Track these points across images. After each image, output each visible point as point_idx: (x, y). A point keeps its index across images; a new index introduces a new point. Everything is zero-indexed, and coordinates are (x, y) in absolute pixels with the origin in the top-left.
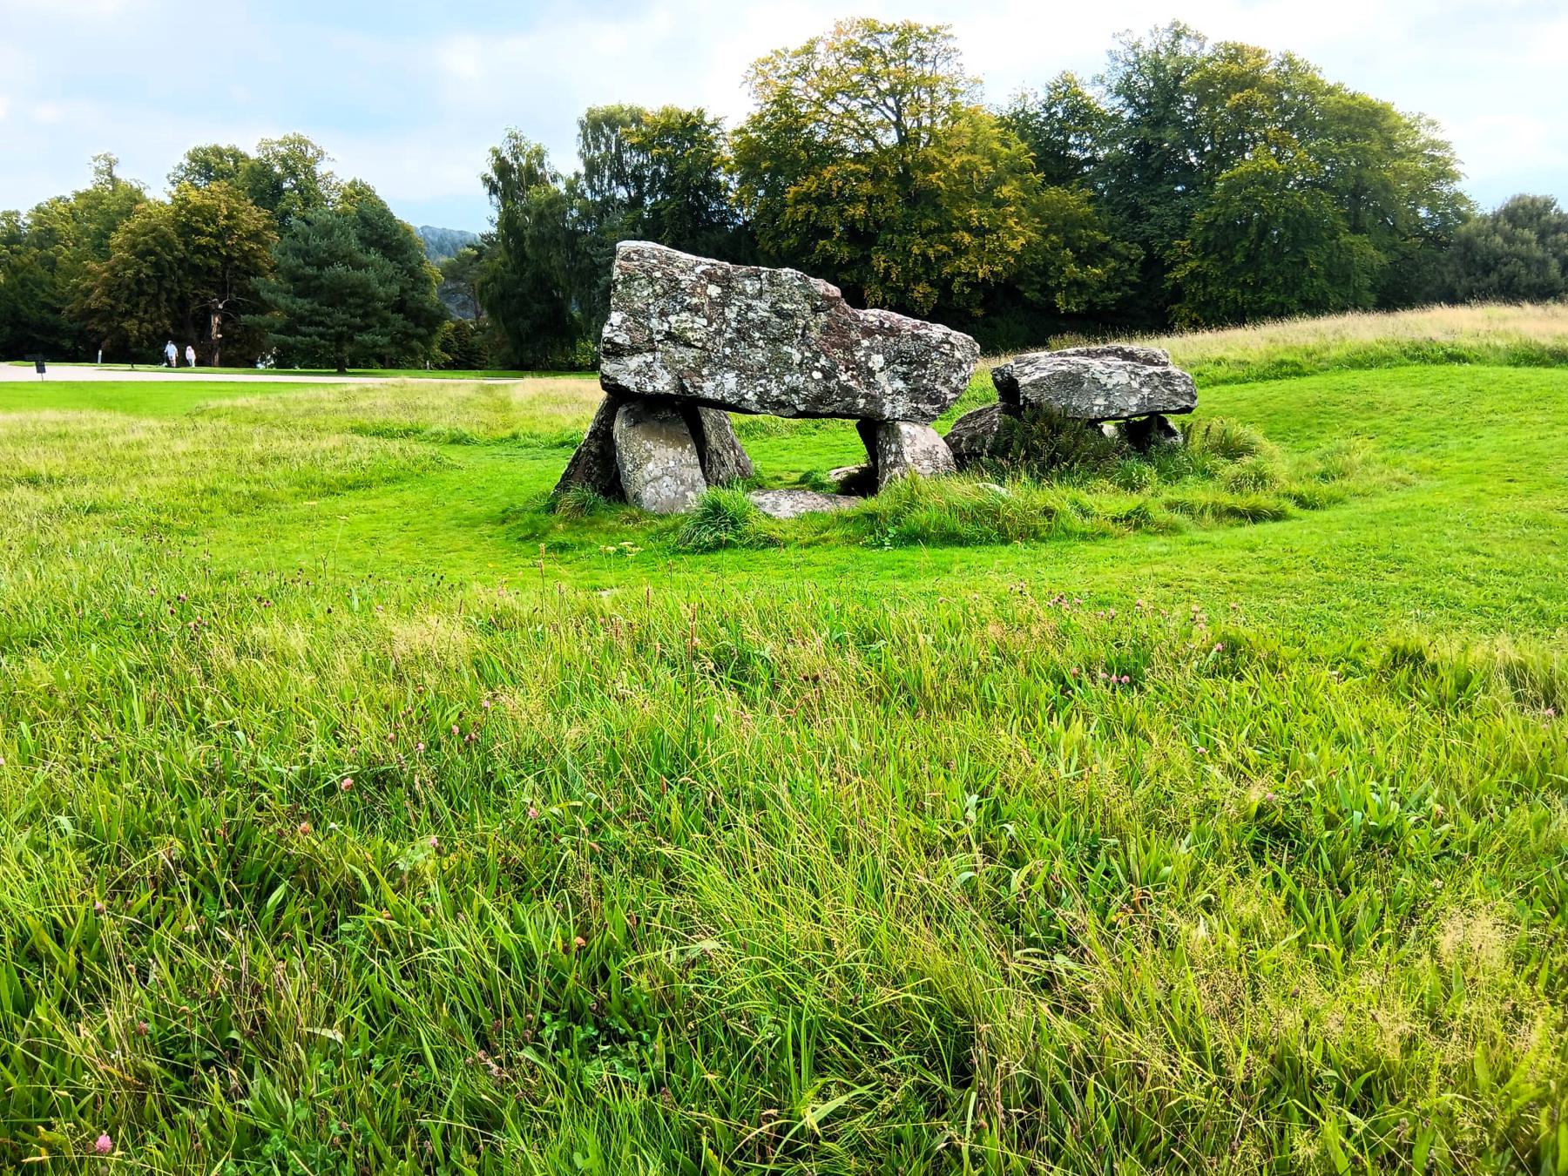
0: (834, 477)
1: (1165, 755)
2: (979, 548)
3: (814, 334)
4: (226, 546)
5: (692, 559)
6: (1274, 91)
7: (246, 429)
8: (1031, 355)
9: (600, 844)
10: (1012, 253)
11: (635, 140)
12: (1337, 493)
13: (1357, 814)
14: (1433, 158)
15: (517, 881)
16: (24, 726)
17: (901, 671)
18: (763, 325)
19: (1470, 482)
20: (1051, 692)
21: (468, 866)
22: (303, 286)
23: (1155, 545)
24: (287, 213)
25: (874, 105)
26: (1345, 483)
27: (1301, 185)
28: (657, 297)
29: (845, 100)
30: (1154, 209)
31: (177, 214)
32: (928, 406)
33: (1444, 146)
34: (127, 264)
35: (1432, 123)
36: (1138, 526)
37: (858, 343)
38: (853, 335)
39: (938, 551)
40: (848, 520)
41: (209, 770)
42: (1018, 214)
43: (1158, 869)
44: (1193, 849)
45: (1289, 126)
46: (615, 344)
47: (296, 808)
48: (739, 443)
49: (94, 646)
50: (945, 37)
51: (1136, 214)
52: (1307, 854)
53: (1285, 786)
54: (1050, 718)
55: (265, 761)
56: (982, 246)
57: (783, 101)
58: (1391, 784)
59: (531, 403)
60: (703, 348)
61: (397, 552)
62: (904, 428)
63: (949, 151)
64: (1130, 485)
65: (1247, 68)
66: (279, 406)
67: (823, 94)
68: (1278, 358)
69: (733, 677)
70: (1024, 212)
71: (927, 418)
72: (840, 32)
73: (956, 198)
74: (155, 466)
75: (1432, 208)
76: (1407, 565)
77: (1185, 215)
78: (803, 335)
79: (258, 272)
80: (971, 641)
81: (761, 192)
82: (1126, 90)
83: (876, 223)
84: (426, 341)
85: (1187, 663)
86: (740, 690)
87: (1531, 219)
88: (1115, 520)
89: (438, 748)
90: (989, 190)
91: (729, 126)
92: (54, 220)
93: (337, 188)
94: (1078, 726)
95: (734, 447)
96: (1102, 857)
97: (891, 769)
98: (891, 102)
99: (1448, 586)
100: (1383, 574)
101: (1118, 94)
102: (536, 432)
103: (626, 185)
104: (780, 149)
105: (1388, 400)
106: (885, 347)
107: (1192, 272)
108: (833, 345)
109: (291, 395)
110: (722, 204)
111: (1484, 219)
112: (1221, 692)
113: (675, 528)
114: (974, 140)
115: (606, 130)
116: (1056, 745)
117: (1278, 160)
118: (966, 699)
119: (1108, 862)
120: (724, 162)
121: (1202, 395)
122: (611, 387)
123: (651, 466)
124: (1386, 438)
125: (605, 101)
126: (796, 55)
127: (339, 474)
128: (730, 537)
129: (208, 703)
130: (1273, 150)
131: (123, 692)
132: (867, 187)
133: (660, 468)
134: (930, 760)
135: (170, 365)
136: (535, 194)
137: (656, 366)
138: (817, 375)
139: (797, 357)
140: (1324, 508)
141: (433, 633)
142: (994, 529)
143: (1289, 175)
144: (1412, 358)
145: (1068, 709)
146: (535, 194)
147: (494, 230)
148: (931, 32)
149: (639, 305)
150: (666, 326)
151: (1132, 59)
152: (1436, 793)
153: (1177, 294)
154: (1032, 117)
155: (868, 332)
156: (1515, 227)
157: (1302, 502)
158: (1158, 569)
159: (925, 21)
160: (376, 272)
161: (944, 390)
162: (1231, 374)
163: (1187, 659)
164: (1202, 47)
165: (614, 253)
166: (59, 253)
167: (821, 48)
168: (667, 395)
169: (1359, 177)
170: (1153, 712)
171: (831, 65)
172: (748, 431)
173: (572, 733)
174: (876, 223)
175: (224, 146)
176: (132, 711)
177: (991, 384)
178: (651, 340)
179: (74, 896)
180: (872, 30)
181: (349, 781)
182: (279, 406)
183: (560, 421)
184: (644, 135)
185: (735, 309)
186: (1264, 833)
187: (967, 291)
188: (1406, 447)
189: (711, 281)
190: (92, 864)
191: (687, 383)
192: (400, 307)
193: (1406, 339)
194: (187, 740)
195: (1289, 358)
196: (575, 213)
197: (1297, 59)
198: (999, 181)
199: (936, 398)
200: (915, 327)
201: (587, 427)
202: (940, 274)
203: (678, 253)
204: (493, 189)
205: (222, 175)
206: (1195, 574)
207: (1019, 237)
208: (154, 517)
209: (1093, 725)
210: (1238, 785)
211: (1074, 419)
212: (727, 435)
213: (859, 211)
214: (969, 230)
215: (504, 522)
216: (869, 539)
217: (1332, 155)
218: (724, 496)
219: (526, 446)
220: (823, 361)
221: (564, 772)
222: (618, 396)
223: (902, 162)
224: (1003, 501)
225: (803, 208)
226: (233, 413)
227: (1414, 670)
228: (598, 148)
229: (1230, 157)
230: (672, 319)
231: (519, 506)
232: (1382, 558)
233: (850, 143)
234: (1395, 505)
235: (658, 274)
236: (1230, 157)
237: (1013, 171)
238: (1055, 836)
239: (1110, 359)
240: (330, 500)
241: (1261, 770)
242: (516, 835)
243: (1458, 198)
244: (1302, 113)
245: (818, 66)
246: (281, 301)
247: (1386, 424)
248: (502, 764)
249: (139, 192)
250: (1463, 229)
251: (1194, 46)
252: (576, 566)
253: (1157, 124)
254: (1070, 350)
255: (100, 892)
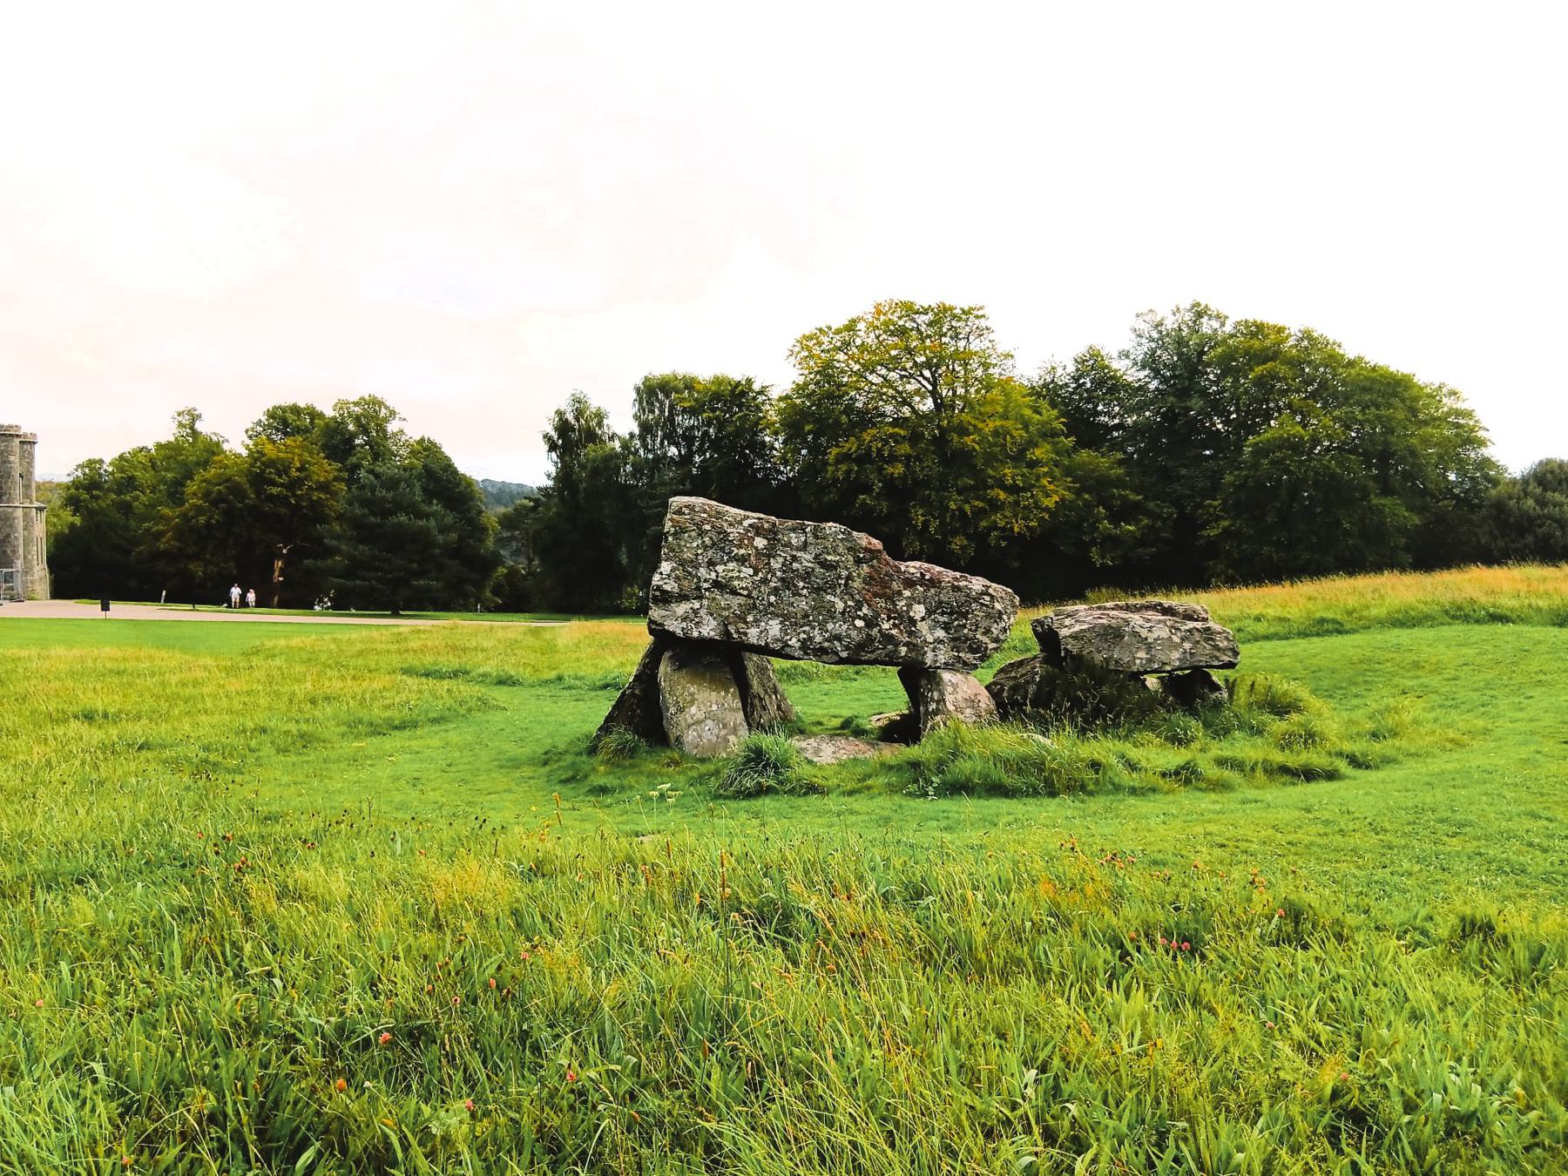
0: (874, 723)
1: (1233, 1030)
2: (1025, 800)
3: (857, 584)
4: (272, 784)
5: (733, 804)
6: (1296, 364)
7: (299, 669)
8: (1070, 608)
9: (639, 1112)
10: (1047, 509)
11: (687, 404)
12: (1390, 752)
13: (1437, 1097)
14: (1458, 426)
15: (551, 1151)
16: (64, 967)
17: (951, 930)
18: (807, 575)
19: (1521, 744)
20: (1110, 958)
21: (502, 1132)
22: (362, 532)
23: (1207, 802)
24: (357, 467)
25: (911, 376)
26: (1397, 743)
27: (1328, 450)
28: (705, 547)
29: (884, 372)
30: (1183, 472)
31: (252, 466)
32: (969, 655)
33: (1468, 414)
34: (199, 510)
35: (1453, 393)
36: (1187, 782)
37: (900, 593)
38: (895, 586)
39: (982, 802)
40: (891, 768)
41: (246, 1019)
42: (1050, 474)
43: (1230, 1156)
44: (1266, 1133)
45: (1314, 396)
46: (665, 592)
47: (332, 1063)
48: (781, 687)
49: (139, 885)
50: (977, 317)
51: (1167, 475)
52: (1387, 1141)
53: (1359, 1065)
54: (1110, 986)
55: (302, 1012)
56: (1017, 503)
57: (826, 371)
58: (1471, 1065)
59: (577, 645)
60: (749, 596)
61: (438, 793)
62: (946, 676)
63: (982, 417)
64: (1177, 740)
65: (1268, 343)
66: (333, 647)
67: (863, 365)
68: (1318, 615)
69: (776, 932)
70: (1057, 472)
71: (969, 667)
72: (879, 312)
73: (990, 458)
74: (209, 705)
75: (1461, 472)
76: (1467, 829)
77: (1215, 477)
78: (846, 585)
79: (324, 519)
80: (1021, 898)
81: (804, 452)
82: (1150, 363)
83: (914, 480)
84: (480, 586)
85: (1249, 930)
86: (784, 946)
87: (1560, 483)
88: (1164, 775)
89: (475, 1003)
90: (1022, 452)
91: (775, 394)
92: (135, 468)
93: (407, 444)
94: (1139, 996)
95: (776, 692)
96: (1171, 1142)
97: (944, 1038)
98: (927, 373)
99: (1513, 852)
100: (1445, 838)
101: (1143, 367)
102: (581, 674)
103: (677, 445)
104: (823, 412)
105: (1434, 660)
106: (925, 597)
107: (1225, 530)
108: (876, 595)
109: (344, 636)
110: (766, 461)
111: (1514, 482)
112: (1286, 962)
113: (717, 773)
114: (1006, 408)
115: (661, 396)
116: (1118, 1017)
117: (1305, 426)
118: (1019, 962)
119: (1178, 1147)
120: (770, 425)
121: (1242, 648)
122: (657, 631)
123: (693, 710)
124: (1434, 697)
125: (663, 367)
126: (838, 332)
127: (388, 714)
128: (772, 783)
129: (248, 948)
130: (1298, 418)
131: (165, 935)
132: (905, 449)
133: (703, 713)
134: (984, 1030)
135: (230, 606)
136: (591, 451)
137: (703, 612)
138: (859, 623)
139: (840, 606)
140: (1377, 768)
141: (487, 881)
142: (1044, 782)
143: (1315, 441)
144: (1454, 617)
145: (1128, 976)
146: (591, 451)
147: (550, 483)
148: (964, 312)
149: (688, 555)
150: (713, 575)
151: (1155, 335)
152: (1519, 1075)
153: (1212, 549)
154: (1061, 387)
155: (909, 583)
156: (1545, 490)
157: (1354, 761)
158: (1211, 828)
159: (959, 302)
160: (436, 519)
161: (985, 639)
162: (1272, 630)
163: (1250, 925)
164: (1223, 325)
165: (666, 506)
166: (136, 499)
167: (861, 326)
168: (712, 640)
169: (1386, 443)
170: (1216, 982)
171: (871, 340)
172: (789, 676)
173: (610, 991)
174: (914, 480)
175: (302, 405)
176: (172, 954)
177: (1029, 633)
178: (698, 588)
179: (101, 1150)
180: (909, 309)
181: (386, 1035)
182: (333, 647)
183: (605, 664)
184: (696, 400)
185: (781, 560)
186: (1339, 1116)
187: (1003, 544)
188: (1456, 707)
189: (758, 534)
190: (121, 1116)
191: (732, 629)
192: (456, 552)
193: (1446, 598)
194: (225, 984)
195: (1330, 615)
196: (629, 468)
197: (1315, 335)
198: (1032, 444)
199: (976, 648)
200: (956, 579)
201: (634, 670)
202: (977, 527)
203: (727, 508)
204: (553, 447)
205: (298, 431)
206: (1250, 834)
207: (1052, 495)
208: (202, 754)
209: (1156, 995)
210: (1310, 1064)
211: (1117, 672)
212: (769, 678)
213: (899, 469)
214: (1004, 487)
215: (545, 763)
216: (912, 788)
217: (1356, 421)
218: (765, 741)
219: (570, 688)
220: (865, 610)
221: (602, 1033)
222: (663, 640)
223: (939, 427)
224: (1048, 751)
225: (844, 467)
226: (288, 653)
227: (1485, 941)
228: (652, 411)
229: (1255, 424)
230: (720, 568)
231: (562, 747)
232: (1442, 821)
233: (889, 409)
234: (1449, 766)
235: (708, 527)
236: (1255, 424)
237: (1044, 435)
238: (1120, 1118)
239: (1150, 614)
240: (375, 740)
241: (1333, 1046)
242: (551, 1100)
243: (1486, 463)
244: (1324, 385)
245: (858, 342)
246: (344, 547)
247: (1434, 684)
248: (539, 1020)
249: (218, 444)
250: (1493, 492)
251: (1216, 324)
252: (617, 810)
253: (1183, 394)
254: (1110, 604)
255: (128, 1148)
